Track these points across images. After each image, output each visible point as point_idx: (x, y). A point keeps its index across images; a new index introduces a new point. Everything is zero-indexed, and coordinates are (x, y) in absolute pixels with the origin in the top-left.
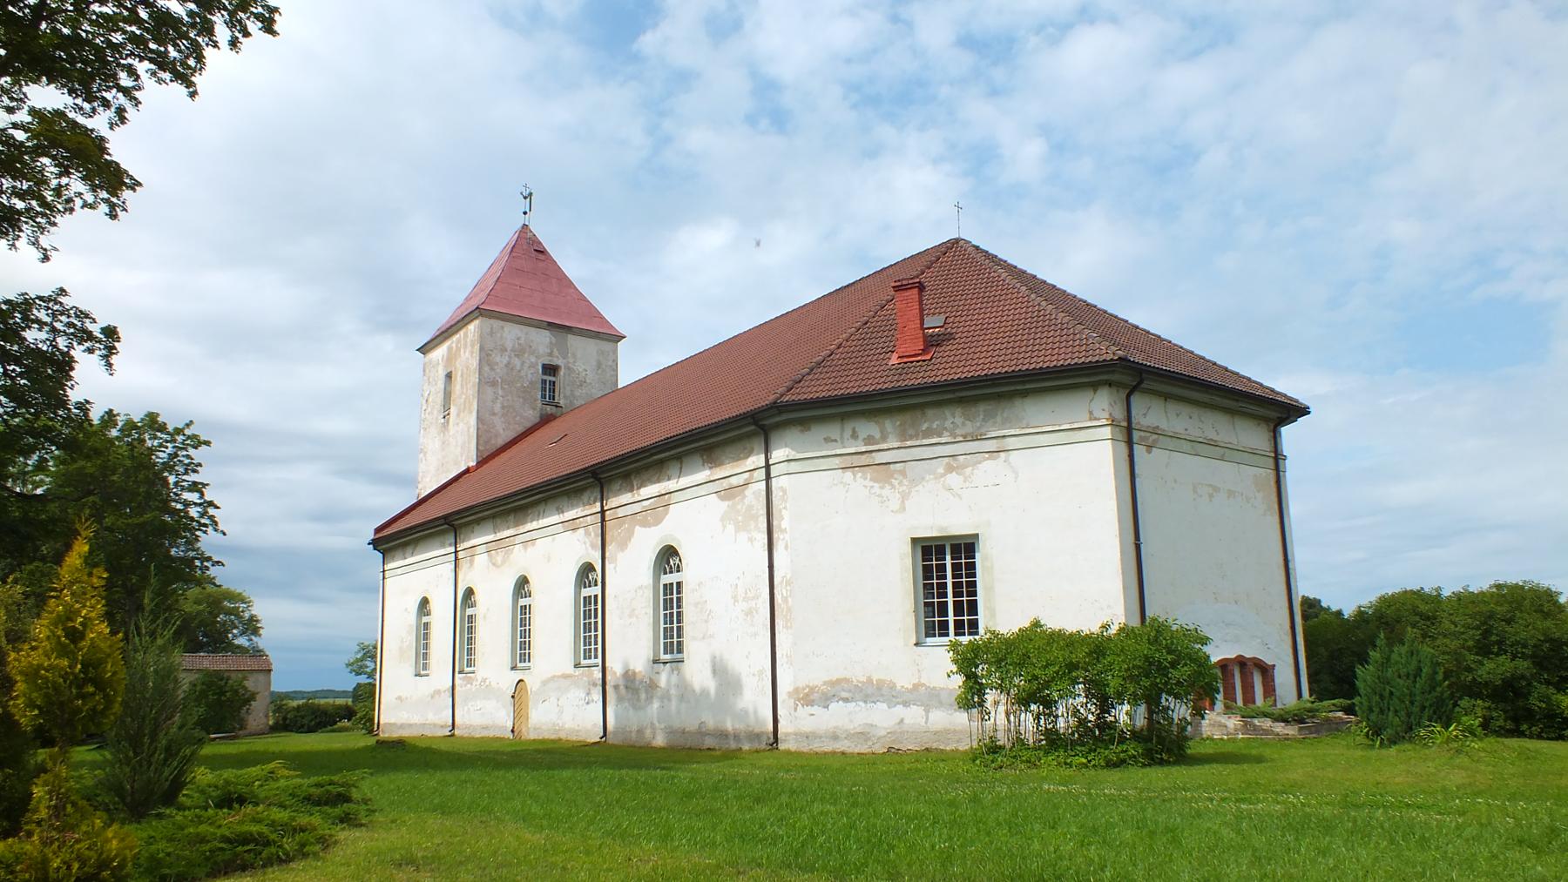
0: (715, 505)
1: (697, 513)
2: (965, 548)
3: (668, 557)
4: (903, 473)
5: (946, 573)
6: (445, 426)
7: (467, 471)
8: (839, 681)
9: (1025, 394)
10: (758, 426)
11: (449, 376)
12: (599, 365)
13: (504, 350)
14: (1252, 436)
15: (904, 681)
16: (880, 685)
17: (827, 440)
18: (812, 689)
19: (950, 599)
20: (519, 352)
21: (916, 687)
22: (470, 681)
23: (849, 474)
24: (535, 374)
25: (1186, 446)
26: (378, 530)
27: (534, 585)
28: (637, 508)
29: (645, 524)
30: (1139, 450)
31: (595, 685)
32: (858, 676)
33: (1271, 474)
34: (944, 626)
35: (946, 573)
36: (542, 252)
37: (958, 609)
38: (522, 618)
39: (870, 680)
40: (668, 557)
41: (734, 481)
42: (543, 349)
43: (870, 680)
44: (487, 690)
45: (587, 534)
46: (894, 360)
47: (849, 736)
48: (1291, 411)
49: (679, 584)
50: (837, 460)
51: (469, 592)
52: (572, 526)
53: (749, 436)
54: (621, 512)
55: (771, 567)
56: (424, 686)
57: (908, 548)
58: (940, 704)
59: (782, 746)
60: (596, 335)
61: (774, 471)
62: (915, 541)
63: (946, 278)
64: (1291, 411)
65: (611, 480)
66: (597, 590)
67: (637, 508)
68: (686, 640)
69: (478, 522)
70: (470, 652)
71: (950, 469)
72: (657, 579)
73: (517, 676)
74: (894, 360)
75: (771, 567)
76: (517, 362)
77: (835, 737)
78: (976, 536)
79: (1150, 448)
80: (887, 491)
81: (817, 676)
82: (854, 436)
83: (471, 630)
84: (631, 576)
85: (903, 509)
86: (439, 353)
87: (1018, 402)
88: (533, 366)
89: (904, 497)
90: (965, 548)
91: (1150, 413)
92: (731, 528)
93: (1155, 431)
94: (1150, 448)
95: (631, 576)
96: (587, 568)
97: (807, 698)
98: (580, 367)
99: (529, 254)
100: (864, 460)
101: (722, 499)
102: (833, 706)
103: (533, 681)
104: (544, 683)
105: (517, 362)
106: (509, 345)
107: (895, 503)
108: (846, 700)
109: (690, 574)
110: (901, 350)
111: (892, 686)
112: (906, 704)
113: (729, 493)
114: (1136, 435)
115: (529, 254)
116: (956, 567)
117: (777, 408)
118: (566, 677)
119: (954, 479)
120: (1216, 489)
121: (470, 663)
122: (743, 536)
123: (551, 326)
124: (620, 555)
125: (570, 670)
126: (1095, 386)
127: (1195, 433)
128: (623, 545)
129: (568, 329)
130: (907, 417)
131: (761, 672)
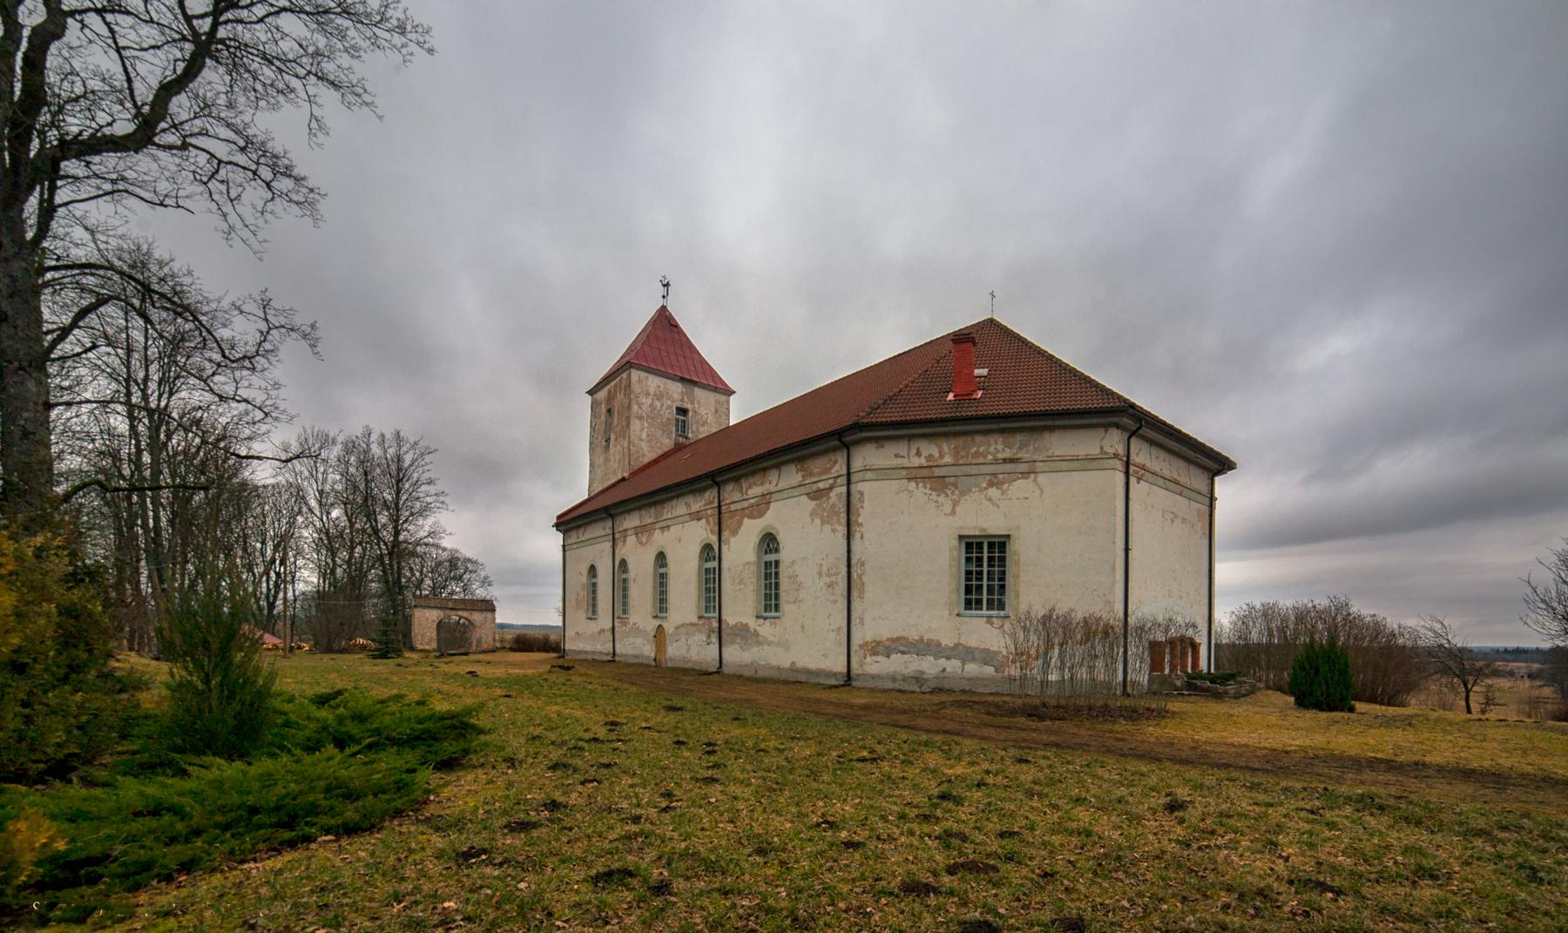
0: (808, 504)
1: (792, 514)
2: (999, 545)
3: (769, 542)
4: (955, 485)
5: (985, 568)
6: (607, 447)
7: (623, 479)
8: (898, 639)
9: (1052, 429)
10: (844, 438)
11: (609, 411)
12: (717, 411)
13: (648, 394)
14: (1197, 480)
15: (948, 641)
16: (929, 643)
17: (897, 456)
18: (878, 643)
19: (985, 583)
20: (659, 397)
21: (957, 645)
22: (625, 624)
23: (913, 484)
24: (669, 414)
25: (1161, 482)
26: (559, 517)
27: (670, 558)
28: (745, 504)
29: (752, 517)
30: (1133, 480)
31: (837, 514)
32: (913, 635)
33: (1206, 509)
34: (979, 602)
35: (985, 568)
36: (676, 326)
37: (990, 590)
38: (662, 581)
39: (922, 640)
40: (769, 542)
41: (821, 485)
42: (676, 396)
43: (922, 640)
44: (637, 631)
45: (708, 522)
46: (951, 396)
47: (904, 679)
48: (1218, 464)
49: (777, 563)
50: (904, 473)
51: (623, 562)
52: (697, 516)
53: (835, 449)
54: (733, 507)
55: (849, 551)
56: (594, 627)
57: (955, 543)
58: (974, 660)
59: (854, 683)
60: (715, 389)
61: (854, 478)
62: (961, 537)
63: (981, 342)
64: (1218, 464)
65: (725, 482)
66: (715, 564)
67: (745, 504)
68: (782, 602)
69: (628, 512)
70: (625, 604)
71: (991, 484)
72: (759, 558)
73: (658, 623)
74: (951, 396)
75: (849, 551)
76: (658, 404)
77: (894, 680)
78: (1008, 536)
79: (1139, 479)
80: (942, 499)
81: (885, 633)
82: (918, 454)
83: (625, 589)
84: (741, 550)
85: (953, 512)
86: (602, 394)
87: (1047, 435)
88: (669, 407)
89: (955, 504)
90: (999, 545)
91: (1142, 454)
92: (818, 521)
93: (1143, 467)
94: (1139, 479)
95: (741, 550)
96: (707, 548)
97: (879, 648)
98: (703, 411)
99: (664, 326)
100: (925, 472)
101: (812, 499)
102: (893, 656)
103: (669, 627)
104: (677, 628)
105: (658, 404)
106: (652, 390)
107: (948, 508)
108: (903, 653)
109: (785, 555)
110: (959, 391)
111: (939, 644)
112: (948, 658)
113: (817, 495)
114: (1132, 468)
115: (664, 326)
116: (991, 559)
117: (857, 427)
118: (692, 624)
119: (993, 492)
120: (1176, 516)
121: (625, 612)
122: (827, 528)
123: (682, 380)
124: (733, 540)
125: (695, 620)
126: (1106, 427)
127: (1166, 473)
128: (735, 532)
129: (695, 383)
130: (960, 441)
131: (839, 629)
